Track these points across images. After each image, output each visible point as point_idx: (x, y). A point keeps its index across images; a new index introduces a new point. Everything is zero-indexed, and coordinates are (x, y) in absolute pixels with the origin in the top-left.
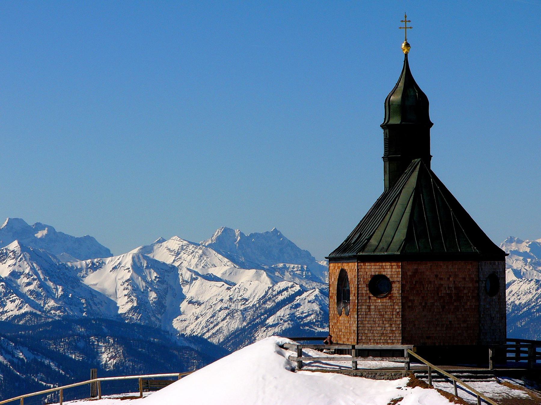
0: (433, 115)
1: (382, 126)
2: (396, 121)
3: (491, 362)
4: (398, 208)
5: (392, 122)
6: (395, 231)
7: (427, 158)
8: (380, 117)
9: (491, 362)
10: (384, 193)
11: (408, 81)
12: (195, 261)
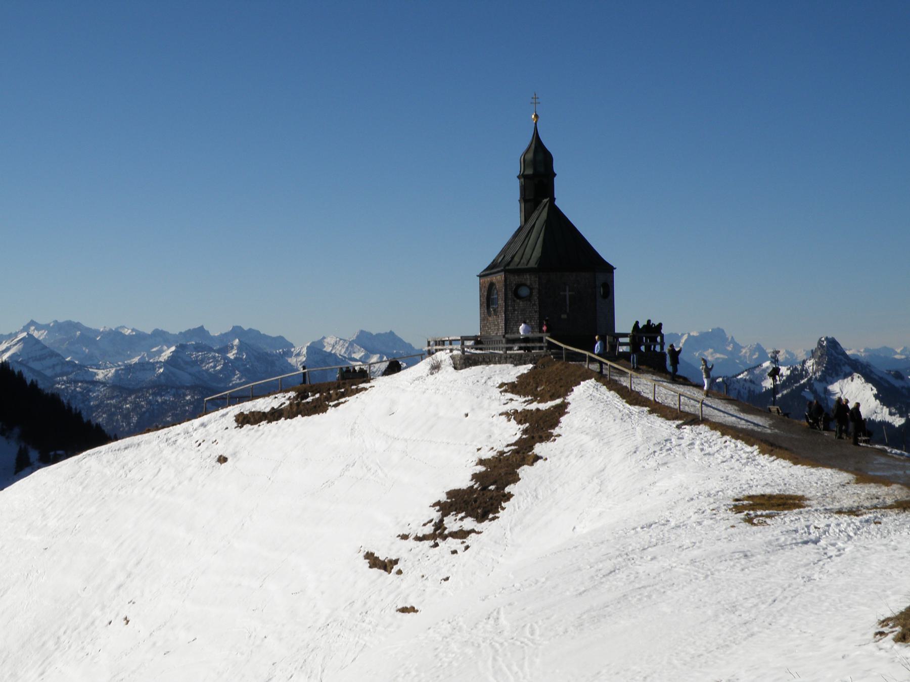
0: (556, 168)
2: (530, 172)
5: (526, 173)
6: (534, 254)
11: (537, 137)
12: (343, 351)
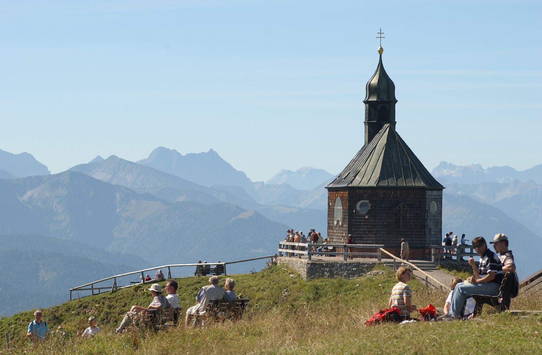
0: (398, 95)
1: (364, 102)
2: (374, 99)
3: (433, 257)
4: (373, 162)
7: (393, 123)
8: (363, 94)
9: (433, 257)
10: (364, 146)
